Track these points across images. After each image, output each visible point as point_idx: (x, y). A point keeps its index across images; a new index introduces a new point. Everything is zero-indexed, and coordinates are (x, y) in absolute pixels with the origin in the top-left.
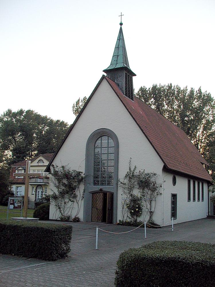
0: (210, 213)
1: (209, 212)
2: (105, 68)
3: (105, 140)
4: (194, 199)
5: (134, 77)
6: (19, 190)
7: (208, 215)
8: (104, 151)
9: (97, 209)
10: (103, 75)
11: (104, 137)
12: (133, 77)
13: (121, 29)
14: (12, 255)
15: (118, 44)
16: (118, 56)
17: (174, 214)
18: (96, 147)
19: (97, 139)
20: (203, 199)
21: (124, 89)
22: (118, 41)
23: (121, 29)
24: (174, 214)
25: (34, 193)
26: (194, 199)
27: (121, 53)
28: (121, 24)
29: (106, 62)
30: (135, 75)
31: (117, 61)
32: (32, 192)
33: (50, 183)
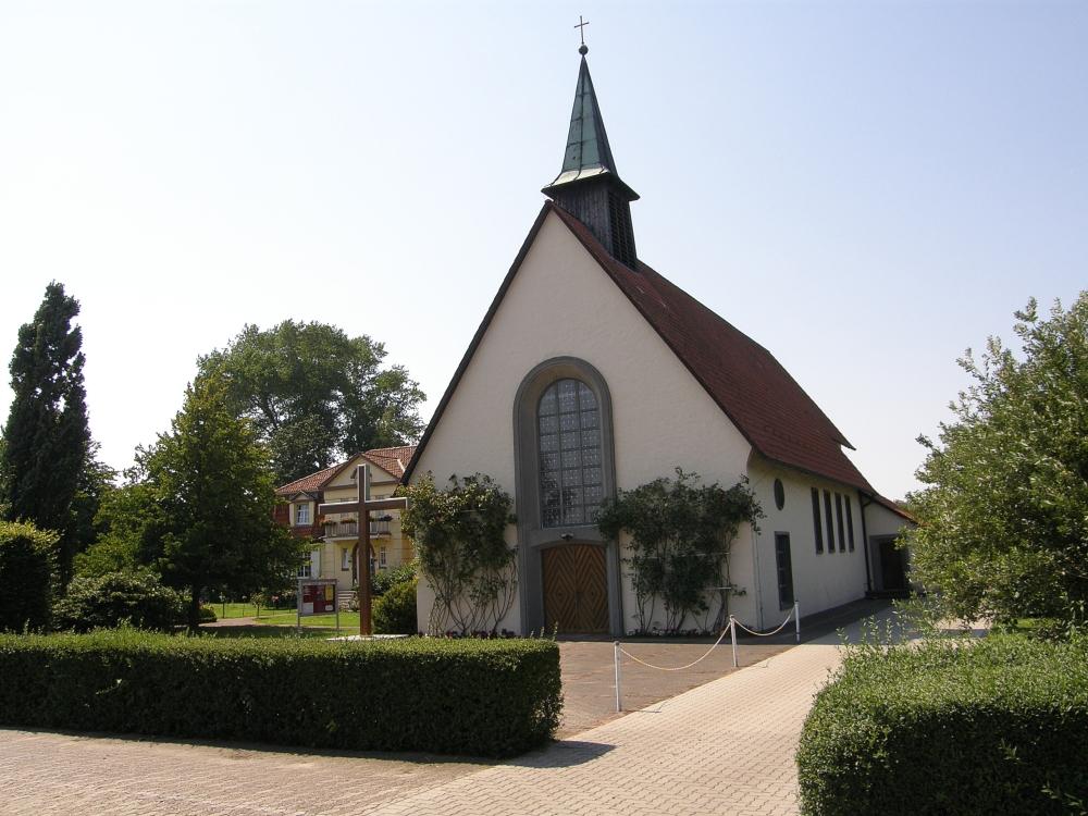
0: (872, 584)
2: (547, 183)
3: (567, 395)
4: (832, 548)
5: (632, 204)
6: (364, 389)
7: (867, 589)
8: (571, 459)
9: (560, 595)
10: (547, 202)
12: (631, 203)
15: (579, 109)
16: (582, 143)
17: (786, 596)
19: (546, 391)
20: (852, 547)
21: (609, 239)
22: (580, 99)
24: (786, 596)
25: (349, 565)
26: (832, 548)
27: (590, 134)
28: (584, 50)
29: (549, 165)
30: (635, 197)
31: (581, 158)
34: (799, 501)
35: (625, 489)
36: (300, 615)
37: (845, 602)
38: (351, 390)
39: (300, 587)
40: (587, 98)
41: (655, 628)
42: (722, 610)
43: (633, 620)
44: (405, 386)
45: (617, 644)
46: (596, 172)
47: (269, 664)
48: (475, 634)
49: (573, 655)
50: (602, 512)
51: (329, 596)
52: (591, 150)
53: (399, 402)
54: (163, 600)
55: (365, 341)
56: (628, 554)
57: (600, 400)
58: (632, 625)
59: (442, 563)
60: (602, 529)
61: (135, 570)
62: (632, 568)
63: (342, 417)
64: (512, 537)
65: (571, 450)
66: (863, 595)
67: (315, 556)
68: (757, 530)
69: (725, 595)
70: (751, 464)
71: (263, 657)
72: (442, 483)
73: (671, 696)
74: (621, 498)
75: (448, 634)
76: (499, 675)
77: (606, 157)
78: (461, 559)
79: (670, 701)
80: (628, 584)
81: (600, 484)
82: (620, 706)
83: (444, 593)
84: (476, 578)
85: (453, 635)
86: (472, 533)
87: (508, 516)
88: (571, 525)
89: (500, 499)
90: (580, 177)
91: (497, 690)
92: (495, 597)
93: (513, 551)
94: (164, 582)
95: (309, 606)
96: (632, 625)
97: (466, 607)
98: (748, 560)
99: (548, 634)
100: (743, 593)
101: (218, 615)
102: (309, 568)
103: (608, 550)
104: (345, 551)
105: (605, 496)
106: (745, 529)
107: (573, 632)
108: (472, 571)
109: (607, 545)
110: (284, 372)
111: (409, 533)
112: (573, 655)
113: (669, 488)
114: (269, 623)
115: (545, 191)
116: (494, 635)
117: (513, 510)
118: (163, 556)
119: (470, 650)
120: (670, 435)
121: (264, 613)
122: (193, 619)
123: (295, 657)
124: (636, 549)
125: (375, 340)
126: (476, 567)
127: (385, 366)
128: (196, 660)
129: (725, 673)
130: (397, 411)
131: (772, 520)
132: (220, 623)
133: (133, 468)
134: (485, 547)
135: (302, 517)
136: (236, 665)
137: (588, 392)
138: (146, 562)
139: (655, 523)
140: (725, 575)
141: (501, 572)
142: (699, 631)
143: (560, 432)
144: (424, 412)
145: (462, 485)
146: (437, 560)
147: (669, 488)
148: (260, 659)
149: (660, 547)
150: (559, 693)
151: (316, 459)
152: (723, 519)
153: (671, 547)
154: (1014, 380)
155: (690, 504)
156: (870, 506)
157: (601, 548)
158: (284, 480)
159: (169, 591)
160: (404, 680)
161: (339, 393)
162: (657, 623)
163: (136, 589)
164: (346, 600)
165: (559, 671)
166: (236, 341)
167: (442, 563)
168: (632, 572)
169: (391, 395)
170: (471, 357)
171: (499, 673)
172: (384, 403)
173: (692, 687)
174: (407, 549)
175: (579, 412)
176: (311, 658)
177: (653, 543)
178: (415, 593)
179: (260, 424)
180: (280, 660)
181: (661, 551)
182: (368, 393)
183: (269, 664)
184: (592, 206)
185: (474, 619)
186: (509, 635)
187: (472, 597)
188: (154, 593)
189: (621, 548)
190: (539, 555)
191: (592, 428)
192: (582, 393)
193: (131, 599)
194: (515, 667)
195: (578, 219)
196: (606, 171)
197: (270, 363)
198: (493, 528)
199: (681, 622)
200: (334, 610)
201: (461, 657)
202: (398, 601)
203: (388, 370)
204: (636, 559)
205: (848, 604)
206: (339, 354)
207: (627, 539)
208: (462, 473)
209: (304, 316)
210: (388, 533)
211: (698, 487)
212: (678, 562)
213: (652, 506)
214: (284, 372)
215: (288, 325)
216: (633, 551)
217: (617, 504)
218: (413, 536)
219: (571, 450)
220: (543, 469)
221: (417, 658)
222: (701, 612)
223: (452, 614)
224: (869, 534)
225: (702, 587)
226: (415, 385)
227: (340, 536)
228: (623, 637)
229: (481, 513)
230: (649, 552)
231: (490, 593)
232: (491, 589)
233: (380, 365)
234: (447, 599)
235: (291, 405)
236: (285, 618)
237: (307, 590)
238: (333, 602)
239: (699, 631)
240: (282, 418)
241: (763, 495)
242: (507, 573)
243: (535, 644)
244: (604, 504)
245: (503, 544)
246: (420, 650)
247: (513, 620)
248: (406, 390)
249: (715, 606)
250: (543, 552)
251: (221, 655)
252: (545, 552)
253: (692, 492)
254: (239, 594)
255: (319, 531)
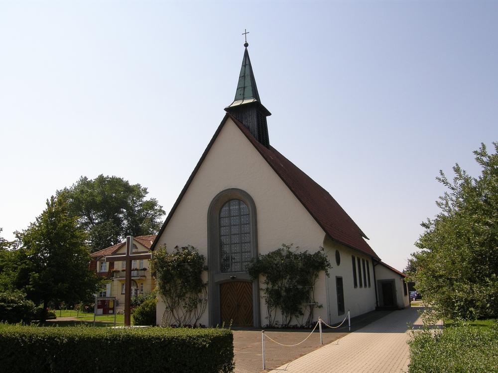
0: (379, 304)
1: (377, 302)
2: (227, 106)
3: (234, 207)
6: (136, 209)
9: (229, 306)
11: (232, 201)
13: (246, 54)
14: (112, 245)
16: (244, 88)
17: (341, 309)
18: (221, 216)
20: (369, 285)
21: (256, 133)
23: (246, 54)
24: (341, 309)
27: (248, 83)
28: (246, 45)
29: (227, 96)
30: (269, 114)
31: (244, 94)
32: (122, 290)
33: (147, 277)
34: (347, 261)
35: (262, 254)
36: (95, 315)
37: (366, 312)
38: (130, 209)
39: (96, 301)
40: (247, 67)
41: (276, 324)
42: (310, 315)
43: (266, 320)
44: (156, 208)
45: (263, 332)
46: (251, 101)
47: (64, 342)
48: (185, 326)
49: (240, 337)
50: (251, 265)
51: (111, 305)
52: (249, 90)
53: (153, 215)
54: (25, 307)
55: (138, 186)
56: (263, 286)
57: (250, 209)
58: (265, 322)
59: (170, 290)
60: (250, 273)
61: (13, 291)
62: (265, 293)
63: (125, 222)
64: (205, 277)
65: (236, 234)
66: (374, 309)
67: (108, 286)
68: (328, 275)
69: (312, 308)
70: (325, 242)
71: (61, 337)
72: (171, 250)
73: (291, 361)
74: (260, 258)
75: (172, 326)
76: (199, 349)
77: (255, 94)
78: (179, 288)
79: (291, 363)
80: (263, 302)
81: (250, 252)
82: (265, 366)
83: (170, 305)
84: (187, 298)
85: (174, 326)
86: (185, 275)
87: (203, 266)
88: (235, 272)
89: (201, 258)
90: (244, 103)
91: (197, 358)
92: (196, 307)
93: (206, 284)
94: (27, 298)
95: (101, 311)
96: (265, 322)
97: (181, 312)
98: (323, 290)
99: (227, 326)
100: (321, 307)
101: (57, 315)
102: (105, 293)
103: (253, 284)
104: (123, 285)
105: (252, 257)
106: (322, 274)
107: (238, 326)
108: (184, 294)
109: (252, 282)
110: (99, 199)
111: (154, 274)
112: (240, 337)
113: (284, 253)
114: (83, 319)
115: (225, 109)
116: (195, 327)
117: (206, 264)
118: (29, 285)
119: (182, 334)
120: (285, 229)
121: (81, 314)
122: (43, 318)
123: (80, 337)
124: (268, 284)
125: (143, 186)
126: (187, 292)
127: (147, 198)
128: (22, 339)
129: (317, 348)
130: (152, 220)
131: (335, 271)
132: (58, 319)
133: (15, 241)
134: (191, 282)
135: (103, 268)
136: (45, 342)
137: (244, 206)
138: (19, 288)
139: (277, 271)
140: (312, 298)
141: (199, 295)
142: (299, 326)
143: (230, 226)
144: (163, 219)
145: (181, 251)
146: (167, 288)
147: (284, 253)
148: (59, 338)
149: (279, 283)
150: (232, 360)
151: (112, 241)
152: (311, 270)
153: (285, 282)
154: (469, 191)
155: (295, 261)
156: (377, 266)
157: (252, 282)
158: (95, 250)
159: (30, 303)
160: (142, 352)
161: (125, 210)
162: (277, 321)
163: (12, 301)
164: (121, 309)
165: (233, 347)
166: (76, 184)
167: (170, 290)
168: (265, 295)
169: (149, 212)
170: (187, 189)
171: (198, 348)
172: (145, 216)
173: (301, 355)
174: (153, 285)
175: (240, 215)
176: (89, 338)
177: (276, 281)
178: (155, 305)
179: (86, 224)
180: (71, 339)
181: (280, 285)
182: (138, 211)
183: (64, 342)
184: (248, 117)
185: (185, 318)
186: (203, 327)
187: (184, 307)
188: (22, 303)
189: (260, 283)
190: (219, 286)
191: (246, 224)
192: (242, 206)
193: (9, 306)
194: (207, 345)
195: (242, 123)
196: (255, 100)
197: (91, 195)
198: (196, 273)
199: (290, 321)
200: (113, 313)
201: (176, 339)
202: (147, 309)
203: (149, 200)
204: (267, 289)
205: (368, 313)
206: (124, 191)
207: (263, 279)
208: (181, 245)
209: (109, 173)
210: (145, 276)
211: (298, 252)
212: (288, 290)
213: (276, 262)
214: (99, 199)
215: (101, 177)
216: (266, 285)
217: (258, 261)
218: (156, 276)
219: (236, 234)
220: (221, 245)
221: (150, 339)
222: (300, 316)
223: (174, 316)
224: (377, 279)
225: (300, 303)
226: (161, 207)
227: (121, 277)
228: (260, 328)
229: (190, 265)
230: (274, 285)
231: (193, 306)
232: (194, 303)
233: (144, 198)
234: (171, 308)
235: (101, 215)
236: (90, 317)
237: (100, 302)
238: (113, 309)
239: (299, 326)
240: (97, 221)
241: (331, 259)
242: (203, 295)
243: (219, 331)
244: (252, 261)
245: (201, 281)
246: (152, 334)
247: (205, 319)
248: (156, 210)
249: (307, 313)
250: (221, 285)
251: (37, 336)
252: (222, 285)
253: (295, 255)
254: (70, 306)
255: (111, 274)
